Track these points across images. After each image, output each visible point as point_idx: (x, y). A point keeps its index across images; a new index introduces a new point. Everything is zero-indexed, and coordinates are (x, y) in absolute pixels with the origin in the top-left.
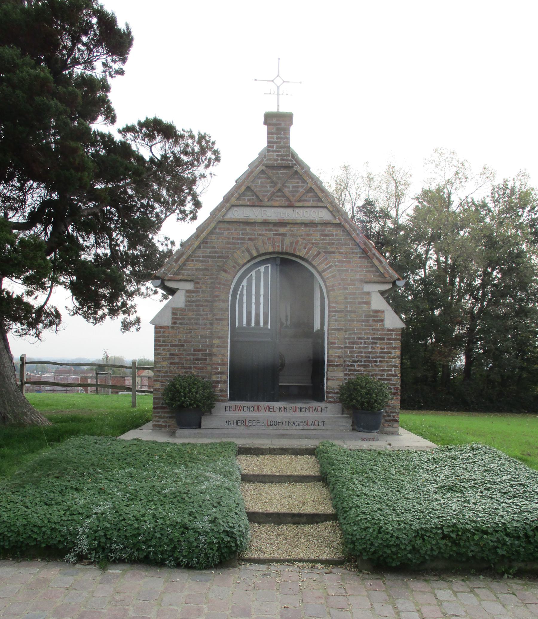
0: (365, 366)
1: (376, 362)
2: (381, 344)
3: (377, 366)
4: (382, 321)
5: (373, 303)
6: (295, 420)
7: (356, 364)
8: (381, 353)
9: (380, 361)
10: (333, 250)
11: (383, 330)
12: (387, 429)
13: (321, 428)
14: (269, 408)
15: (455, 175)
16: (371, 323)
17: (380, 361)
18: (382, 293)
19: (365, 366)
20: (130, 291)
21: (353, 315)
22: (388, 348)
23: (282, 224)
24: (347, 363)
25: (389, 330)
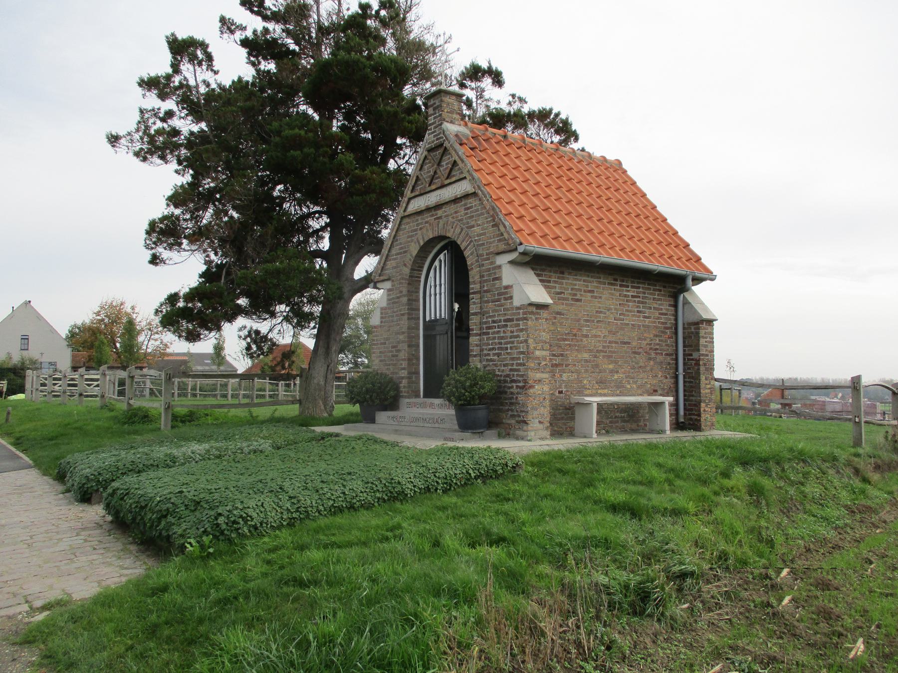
0: (499, 355)
1: (507, 348)
2: (511, 326)
3: (508, 353)
4: (511, 298)
5: (504, 279)
6: (425, 417)
7: (491, 353)
8: (511, 337)
9: (511, 348)
10: (473, 223)
11: (512, 308)
12: (519, 433)
13: (441, 426)
14: (432, 405)
15: (163, 261)
16: (503, 302)
17: (511, 348)
18: (511, 262)
19: (499, 355)
20: (288, 309)
21: (488, 295)
22: (517, 331)
23: (438, 207)
24: (485, 352)
25: (518, 308)
